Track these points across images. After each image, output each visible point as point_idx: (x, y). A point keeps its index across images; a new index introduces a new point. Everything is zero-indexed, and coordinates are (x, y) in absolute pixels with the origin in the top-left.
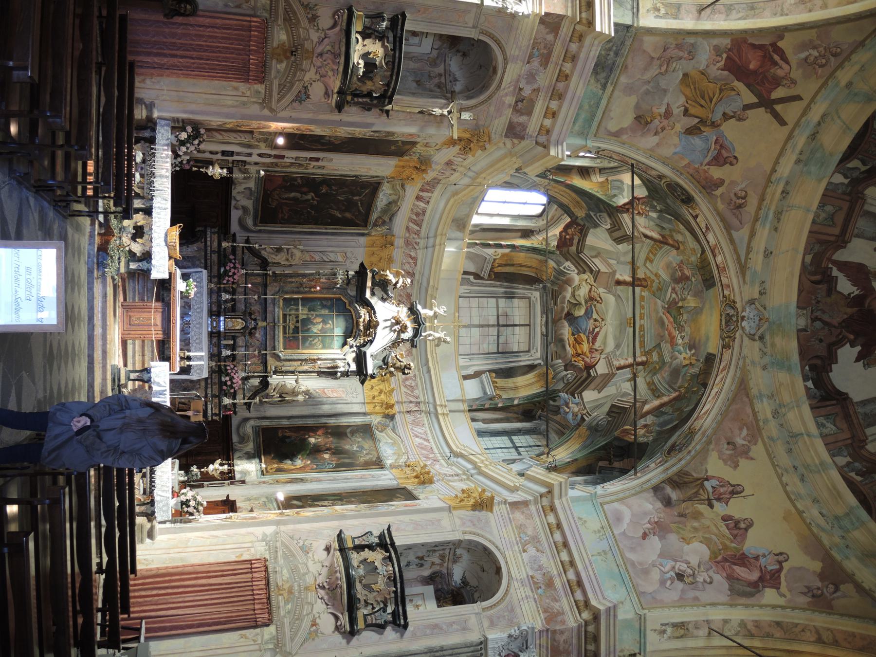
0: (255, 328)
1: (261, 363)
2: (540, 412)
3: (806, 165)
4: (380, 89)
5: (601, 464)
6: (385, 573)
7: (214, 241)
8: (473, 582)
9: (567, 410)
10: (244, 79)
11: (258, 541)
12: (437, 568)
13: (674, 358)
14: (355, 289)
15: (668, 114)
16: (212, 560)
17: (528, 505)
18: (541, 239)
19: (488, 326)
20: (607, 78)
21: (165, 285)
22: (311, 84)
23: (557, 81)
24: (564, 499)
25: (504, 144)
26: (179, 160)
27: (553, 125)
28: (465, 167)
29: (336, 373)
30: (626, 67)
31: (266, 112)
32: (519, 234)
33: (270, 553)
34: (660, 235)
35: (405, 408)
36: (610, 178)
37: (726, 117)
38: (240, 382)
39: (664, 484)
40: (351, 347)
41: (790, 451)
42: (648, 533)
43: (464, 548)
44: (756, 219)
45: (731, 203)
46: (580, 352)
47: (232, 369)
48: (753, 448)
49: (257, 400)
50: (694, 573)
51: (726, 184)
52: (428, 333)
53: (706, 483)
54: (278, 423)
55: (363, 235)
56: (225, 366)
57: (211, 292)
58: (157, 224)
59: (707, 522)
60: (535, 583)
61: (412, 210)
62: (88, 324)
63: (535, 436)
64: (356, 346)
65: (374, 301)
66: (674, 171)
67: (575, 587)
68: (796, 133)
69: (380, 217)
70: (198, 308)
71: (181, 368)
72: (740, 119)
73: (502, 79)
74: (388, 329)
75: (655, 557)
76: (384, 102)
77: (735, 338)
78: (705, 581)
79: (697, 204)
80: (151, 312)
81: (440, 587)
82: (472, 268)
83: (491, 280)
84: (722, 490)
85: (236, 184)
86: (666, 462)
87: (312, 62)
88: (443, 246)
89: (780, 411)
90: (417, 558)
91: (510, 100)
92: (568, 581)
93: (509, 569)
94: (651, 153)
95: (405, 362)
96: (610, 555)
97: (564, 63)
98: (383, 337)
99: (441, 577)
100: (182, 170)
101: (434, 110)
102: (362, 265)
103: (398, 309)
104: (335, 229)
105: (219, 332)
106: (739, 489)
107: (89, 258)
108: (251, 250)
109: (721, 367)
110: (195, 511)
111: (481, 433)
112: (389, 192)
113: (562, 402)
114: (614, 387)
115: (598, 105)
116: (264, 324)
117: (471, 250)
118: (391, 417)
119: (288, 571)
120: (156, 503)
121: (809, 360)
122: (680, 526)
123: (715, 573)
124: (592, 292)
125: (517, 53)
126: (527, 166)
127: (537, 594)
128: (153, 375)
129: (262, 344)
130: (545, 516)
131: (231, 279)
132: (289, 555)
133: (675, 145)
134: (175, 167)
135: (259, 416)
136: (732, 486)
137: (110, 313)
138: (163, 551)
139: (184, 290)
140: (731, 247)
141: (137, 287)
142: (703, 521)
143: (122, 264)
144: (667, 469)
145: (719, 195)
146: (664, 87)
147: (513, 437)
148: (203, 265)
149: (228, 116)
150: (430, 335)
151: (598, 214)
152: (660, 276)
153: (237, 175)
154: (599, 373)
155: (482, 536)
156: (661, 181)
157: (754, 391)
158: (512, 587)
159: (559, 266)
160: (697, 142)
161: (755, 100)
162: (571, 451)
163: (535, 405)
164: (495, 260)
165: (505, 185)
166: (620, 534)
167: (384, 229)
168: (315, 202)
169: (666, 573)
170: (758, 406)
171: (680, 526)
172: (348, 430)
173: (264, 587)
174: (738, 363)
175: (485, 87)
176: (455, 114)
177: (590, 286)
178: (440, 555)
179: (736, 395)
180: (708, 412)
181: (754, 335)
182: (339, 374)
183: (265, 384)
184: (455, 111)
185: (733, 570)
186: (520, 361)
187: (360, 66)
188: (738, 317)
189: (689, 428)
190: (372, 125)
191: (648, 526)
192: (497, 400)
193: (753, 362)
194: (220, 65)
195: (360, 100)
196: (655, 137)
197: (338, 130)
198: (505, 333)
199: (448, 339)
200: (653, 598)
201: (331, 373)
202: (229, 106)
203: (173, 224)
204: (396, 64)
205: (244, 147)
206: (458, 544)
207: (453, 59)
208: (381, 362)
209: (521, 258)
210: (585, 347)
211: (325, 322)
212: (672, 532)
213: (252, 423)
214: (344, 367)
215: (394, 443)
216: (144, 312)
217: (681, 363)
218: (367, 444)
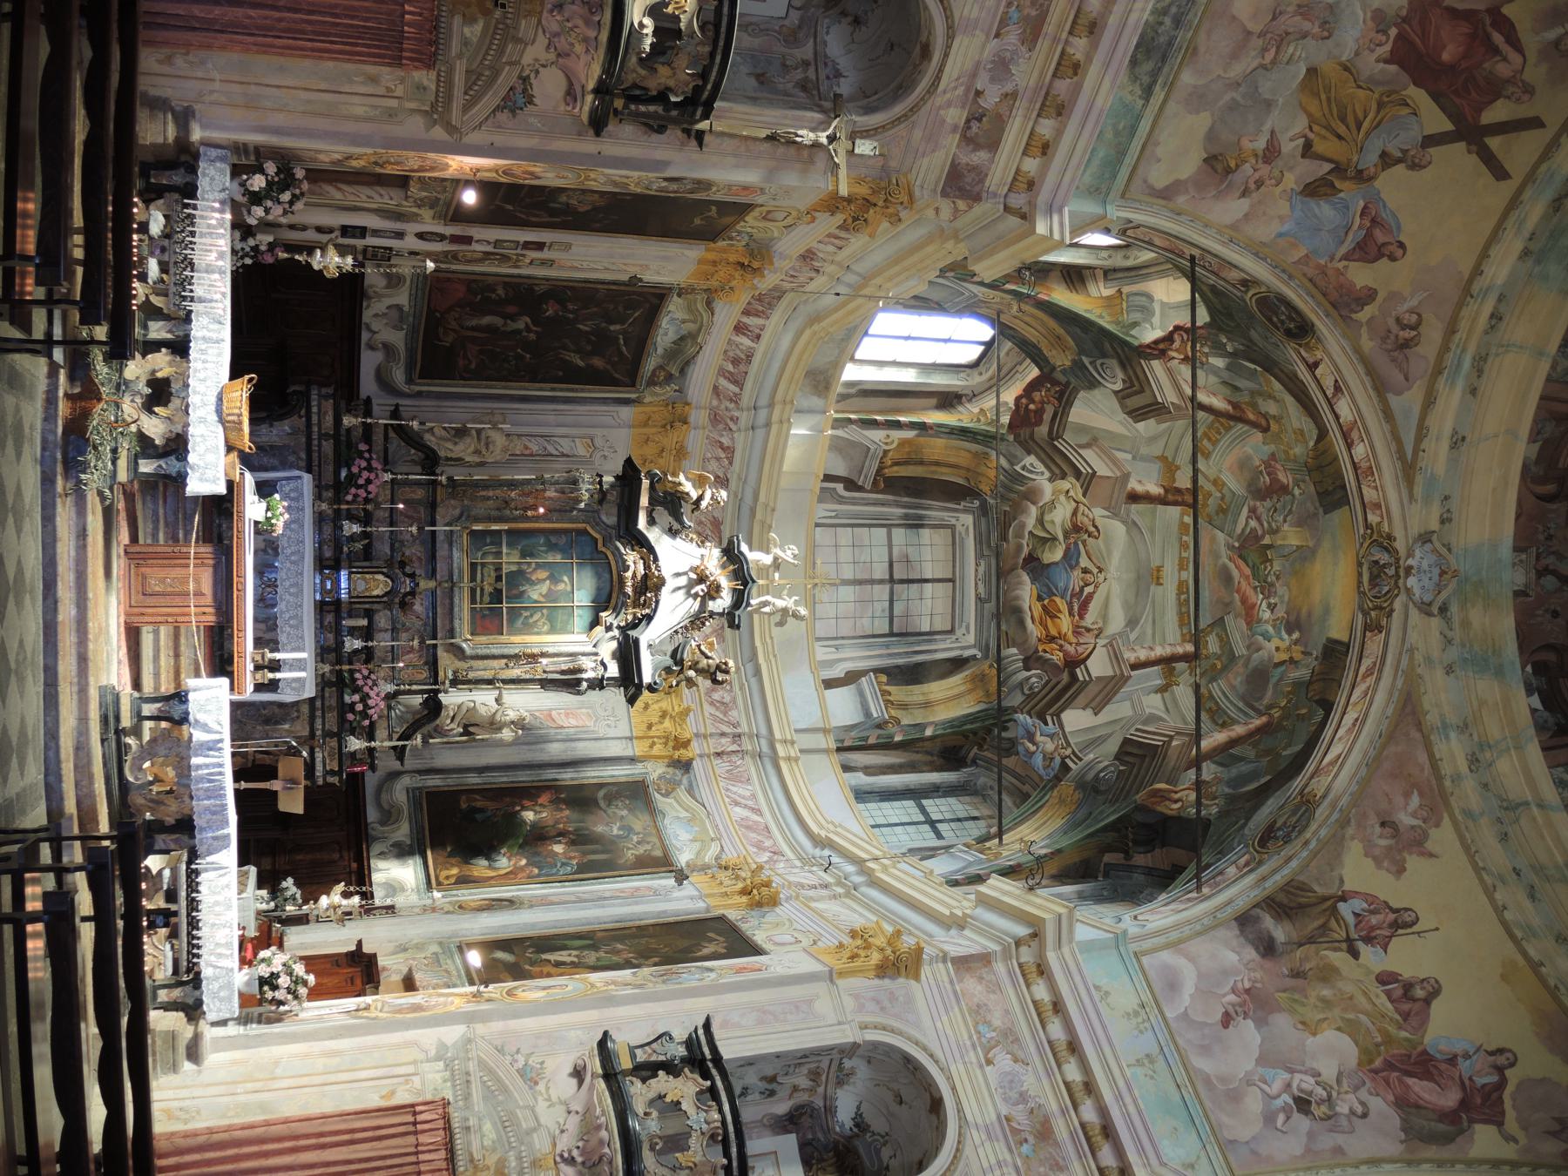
0: (413, 593)
1: (426, 663)
2: (975, 750)
3: (1538, 262)
4: (687, 84)
5: (1108, 858)
6: (705, 1127)
7: (326, 413)
8: (878, 1124)
9: (1032, 748)
10: (391, 57)
11: (428, 1061)
12: (803, 1098)
13: (1253, 647)
14: (615, 511)
15: (1271, 153)
16: (328, 1107)
17: (989, 962)
18: (976, 410)
19: (872, 582)
20: (1154, 75)
21: (220, 509)
22: (537, 72)
23: (1054, 75)
24: (1066, 950)
25: (937, 210)
26: (251, 242)
27: (1044, 170)
28: (839, 264)
29: (579, 681)
30: (1195, 49)
31: (438, 133)
32: (934, 401)
33: (454, 1086)
34: (1230, 402)
35: (713, 745)
36: (1125, 290)
37: (1386, 160)
38: (382, 705)
39: (1259, 910)
40: (609, 628)
41: (1504, 838)
42: (1234, 1015)
43: (862, 1057)
44: (1438, 371)
45: (1388, 337)
46: (1054, 632)
47: (365, 678)
48: (1434, 833)
49: (418, 739)
50: (1330, 1096)
51: (1380, 298)
52: (763, 599)
53: (1341, 906)
54: (458, 781)
55: (626, 402)
56: (351, 672)
57: (320, 519)
58: (201, 375)
59: (1349, 988)
60: (1015, 1132)
61: (725, 352)
62: (45, 598)
63: (967, 799)
64: (619, 627)
65: (654, 536)
66: (1277, 271)
67: (1099, 1140)
68: (1526, 195)
69: (661, 367)
70: (292, 554)
71: (255, 685)
72: (1415, 166)
73: (941, 70)
74: (682, 592)
75: (1249, 1065)
76: (694, 113)
77: (1392, 611)
78: (1352, 1112)
79: (1319, 340)
80: (187, 566)
81: (810, 1136)
82: (840, 469)
83: (877, 493)
84: (1374, 920)
85: (370, 298)
86: (1260, 863)
87: (539, 22)
88: (785, 426)
89: (1480, 757)
90: (764, 1078)
91: (955, 115)
92: (1083, 1126)
93: (959, 1103)
94: (1233, 233)
95: (716, 658)
96: (1161, 1064)
97: (1071, 39)
98: (673, 608)
99: (811, 1116)
100: (257, 265)
101: (800, 132)
102: (629, 462)
103: (702, 551)
104: (572, 390)
105: (338, 602)
106: (1408, 917)
107: (44, 449)
108: (402, 431)
109: (1363, 669)
110: (290, 997)
111: (862, 795)
112: (680, 315)
113: (1021, 732)
114: (1128, 704)
115: (1133, 130)
116: (432, 584)
117: (840, 433)
118: (686, 766)
119: (494, 1124)
120: (204, 983)
121: (1533, 652)
122: (1296, 997)
123: (1371, 1094)
124: (1080, 517)
125: (975, 14)
126: (980, 259)
127: (1020, 1155)
128: (192, 707)
129: (425, 625)
130: (1028, 986)
131: (362, 493)
132: (496, 1090)
133: (1281, 218)
134: (242, 258)
135: (420, 767)
136: (1397, 911)
137: (94, 574)
138: (222, 1089)
139: (261, 518)
140: (1386, 427)
141: (161, 511)
142: (1340, 984)
143: (122, 463)
144: (1264, 879)
145: (1364, 320)
146: (1267, 96)
147: (925, 802)
148: (303, 464)
149: (355, 140)
150: (765, 604)
151: (1099, 362)
152: (1224, 484)
153: (373, 275)
154: (1094, 675)
155: (900, 1033)
156: (1246, 292)
157: (1432, 718)
158: (968, 1142)
159: (1012, 464)
160: (1325, 210)
161: (1448, 126)
162: (1045, 832)
163: (966, 737)
164: (886, 452)
165: (913, 302)
166: (1177, 1018)
167: (669, 391)
168: (532, 336)
169: (1275, 1098)
170: (1440, 749)
171: (1296, 997)
172: (601, 794)
173: (444, 1165)
174: (1399, 662)
175: (902, 89)
176: (842, 147)
177: (1074, 504)
178: (810, 1072)
179: (1396, 726)
180: (1341, 760)
181: (1430, 604)
182: (585, 684)
183: (433, 707)
184: (841, 135)
185: (1408, 1087)
186: (936, 651)
187: (645, 31)
188: (1397, 568)
189: (1301, 793)
190: (664, 164)
191: (1232, 998)
192: (891, 729)
193: (1429, 660)
194: (338, 24)
195: (642, 108)
196: (1242, 200)
197: (592, 175)
198: (904, 597)
199: (803, 611)
200: (1254, 1152)
201: (569, 682)
202: (357, 119)
203: (235, 374)
204: (723, 29)
205: (388, 218)
206: (851, 1050)
207: (834, 29)
208: (668, 658)
209: (937, 447)
210: (1065, 624)
211: (554, 579)
212: (1280, 1009)
213: (406, 781)
214: (594, 669)
215: (692, 820)
216: (175, 566)
217: (1271, 658)
218: (639, 823)
